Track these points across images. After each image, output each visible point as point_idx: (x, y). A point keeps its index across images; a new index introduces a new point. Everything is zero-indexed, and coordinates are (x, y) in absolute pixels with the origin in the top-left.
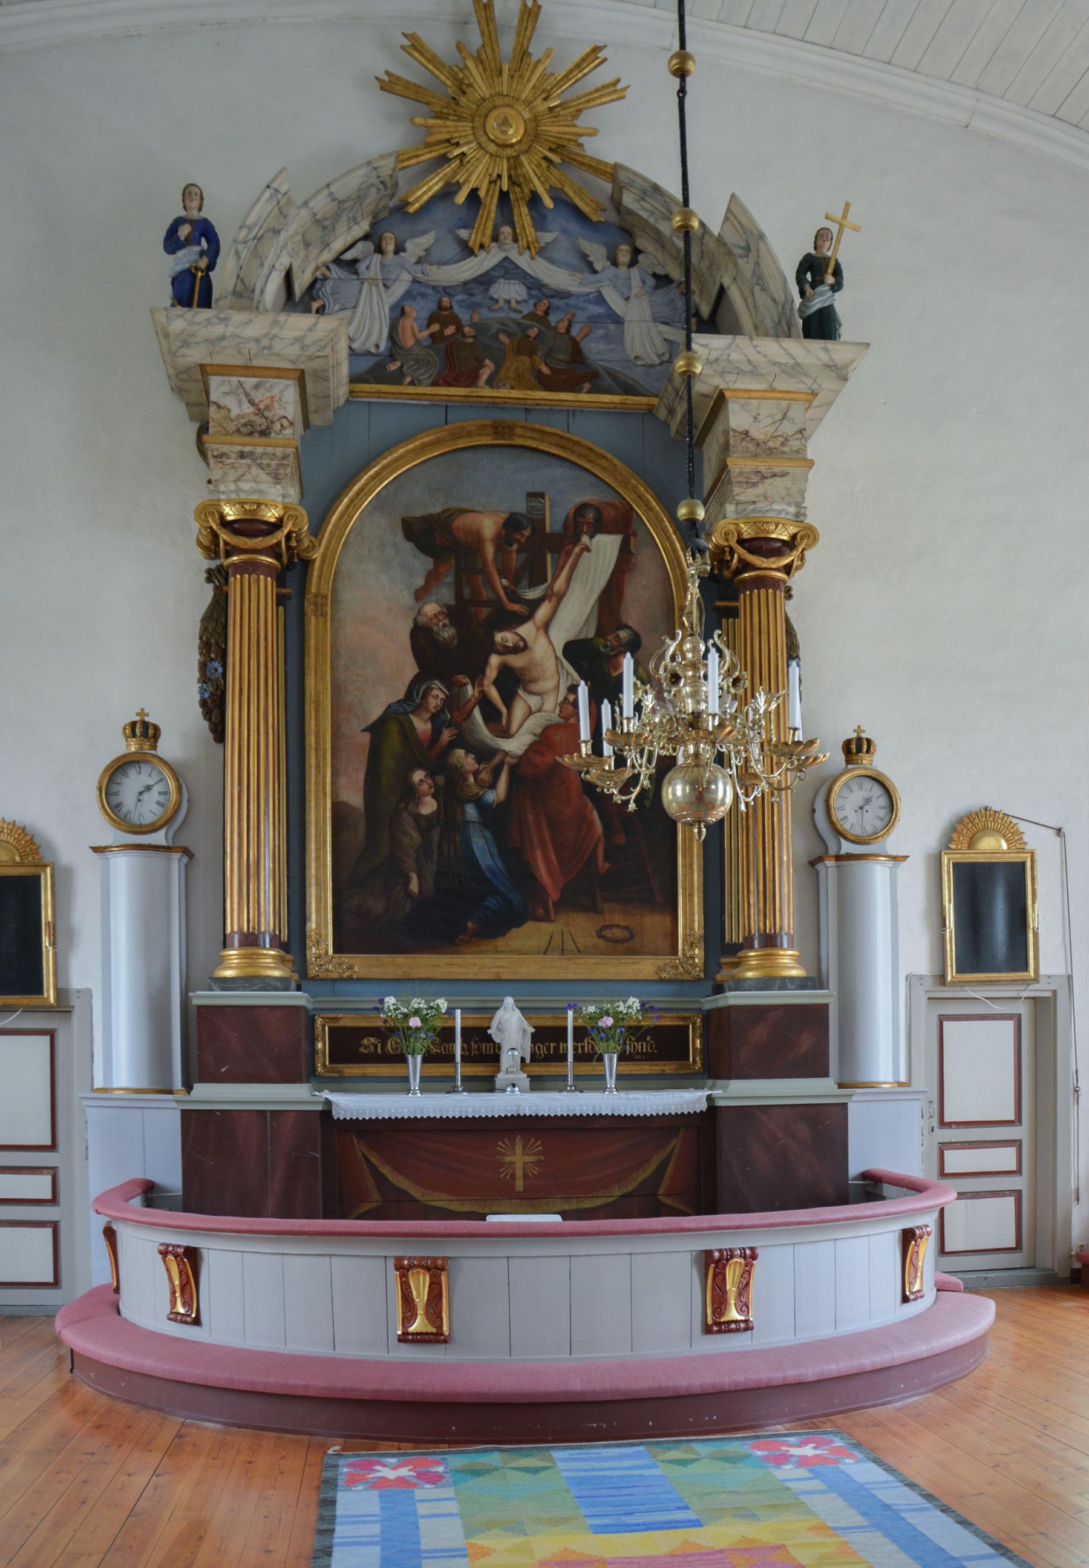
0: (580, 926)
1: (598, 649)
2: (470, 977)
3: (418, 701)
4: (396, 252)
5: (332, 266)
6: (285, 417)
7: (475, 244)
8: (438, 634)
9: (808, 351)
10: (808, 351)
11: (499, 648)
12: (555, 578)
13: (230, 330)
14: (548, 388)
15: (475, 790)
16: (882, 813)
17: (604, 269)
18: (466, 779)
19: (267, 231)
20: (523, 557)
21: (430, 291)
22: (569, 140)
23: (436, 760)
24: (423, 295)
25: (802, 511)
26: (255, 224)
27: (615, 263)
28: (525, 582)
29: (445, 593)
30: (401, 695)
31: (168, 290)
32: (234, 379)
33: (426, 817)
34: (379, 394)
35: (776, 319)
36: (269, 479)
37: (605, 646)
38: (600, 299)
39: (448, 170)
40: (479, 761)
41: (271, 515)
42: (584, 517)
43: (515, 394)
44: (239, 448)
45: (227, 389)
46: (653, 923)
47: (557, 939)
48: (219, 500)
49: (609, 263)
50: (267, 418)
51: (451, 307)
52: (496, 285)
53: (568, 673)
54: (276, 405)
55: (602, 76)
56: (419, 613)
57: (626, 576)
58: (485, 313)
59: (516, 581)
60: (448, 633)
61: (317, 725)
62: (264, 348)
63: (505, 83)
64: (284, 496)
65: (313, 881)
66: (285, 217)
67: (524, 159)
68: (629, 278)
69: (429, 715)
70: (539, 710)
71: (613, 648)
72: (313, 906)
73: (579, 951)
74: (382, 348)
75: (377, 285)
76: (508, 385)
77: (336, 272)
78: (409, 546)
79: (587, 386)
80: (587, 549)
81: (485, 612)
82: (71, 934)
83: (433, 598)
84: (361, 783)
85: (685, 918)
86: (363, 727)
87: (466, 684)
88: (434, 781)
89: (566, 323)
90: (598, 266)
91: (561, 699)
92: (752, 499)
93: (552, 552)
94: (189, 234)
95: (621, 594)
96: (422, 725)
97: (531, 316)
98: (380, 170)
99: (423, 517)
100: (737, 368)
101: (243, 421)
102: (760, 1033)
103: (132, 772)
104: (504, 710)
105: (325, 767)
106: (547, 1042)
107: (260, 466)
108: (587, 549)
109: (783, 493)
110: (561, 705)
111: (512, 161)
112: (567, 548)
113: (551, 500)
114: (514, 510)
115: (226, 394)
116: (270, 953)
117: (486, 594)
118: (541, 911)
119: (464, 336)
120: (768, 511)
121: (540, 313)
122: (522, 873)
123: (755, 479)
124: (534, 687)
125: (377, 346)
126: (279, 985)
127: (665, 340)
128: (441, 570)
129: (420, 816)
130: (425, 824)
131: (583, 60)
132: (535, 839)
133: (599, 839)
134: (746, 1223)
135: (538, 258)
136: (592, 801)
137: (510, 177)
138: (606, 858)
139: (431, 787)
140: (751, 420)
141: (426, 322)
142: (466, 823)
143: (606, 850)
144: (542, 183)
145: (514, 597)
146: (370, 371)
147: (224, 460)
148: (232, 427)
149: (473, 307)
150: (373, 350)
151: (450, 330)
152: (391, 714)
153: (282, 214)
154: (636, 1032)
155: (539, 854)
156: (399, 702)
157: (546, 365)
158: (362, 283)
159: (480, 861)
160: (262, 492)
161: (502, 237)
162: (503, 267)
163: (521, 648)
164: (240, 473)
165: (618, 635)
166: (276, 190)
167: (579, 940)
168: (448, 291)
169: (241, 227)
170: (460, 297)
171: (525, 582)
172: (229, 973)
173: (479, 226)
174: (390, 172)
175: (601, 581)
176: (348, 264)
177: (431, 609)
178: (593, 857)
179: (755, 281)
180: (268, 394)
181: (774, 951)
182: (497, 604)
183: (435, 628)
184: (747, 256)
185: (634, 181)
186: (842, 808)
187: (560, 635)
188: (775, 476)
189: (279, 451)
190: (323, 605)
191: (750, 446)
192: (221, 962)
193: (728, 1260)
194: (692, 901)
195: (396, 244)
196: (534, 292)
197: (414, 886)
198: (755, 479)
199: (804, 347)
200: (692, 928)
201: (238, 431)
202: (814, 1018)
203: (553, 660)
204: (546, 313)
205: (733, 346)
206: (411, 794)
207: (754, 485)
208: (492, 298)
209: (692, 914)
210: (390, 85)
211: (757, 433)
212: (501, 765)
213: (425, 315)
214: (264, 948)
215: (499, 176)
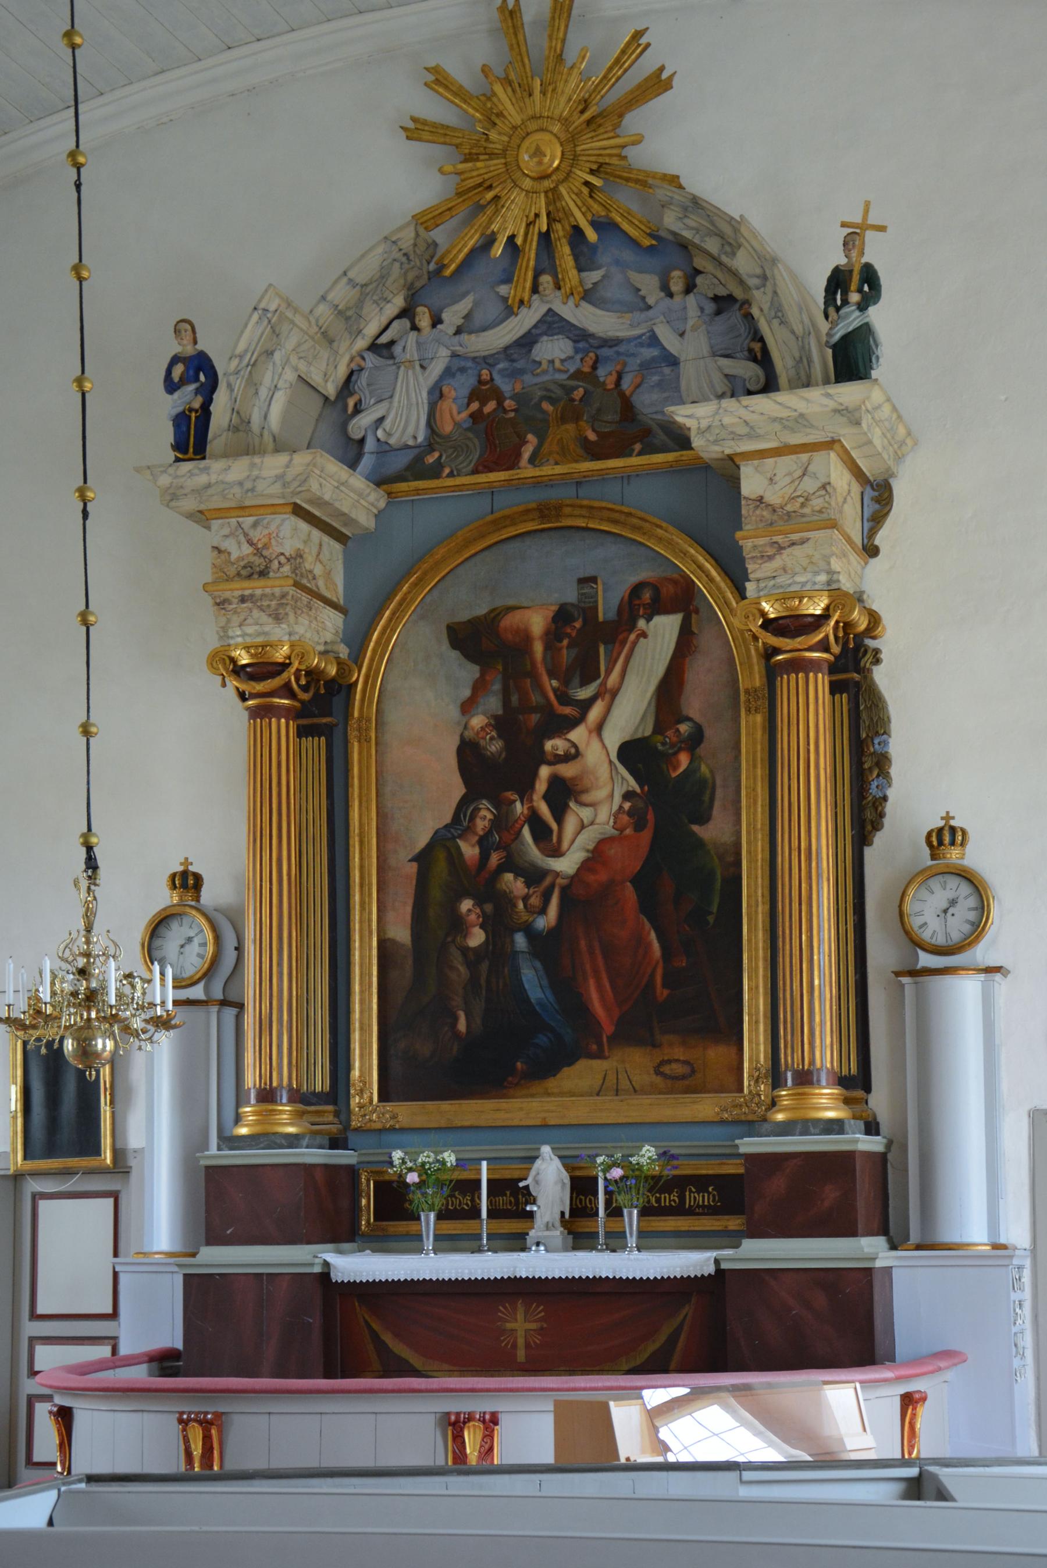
0: (636, 1063)
1: (656, 748)
2: (516, 1122)
3: (465, 824)
4: (434, 326)
5: (366, 355)
6: (282, 554)
7: (514, 300)
8: (485, 749)
9: (807, 400)
10: (807, 400)
11: (550, 758)
12: (609, 672)
13: (214, 478)
14: (596, 457)
15: (525, 917)
16: (972, 916)
17: (657, 303)
18: (515, 906)
19: (260, 355)
20: (574, 652)
21: (470, 364)
22: (610, 155)
23: (484, 887)
24: (462, 370)
25: (835, 577)
26: (246, 351)
27: (670, 295)
28: (576, 680)
29: (493, 703)
30: (448, 819)
31: (168, 434)
32: (233, 521)
33: (474, 949)
34: (417, 491)
35: (797, 355)
36: (270, 620)
37: (664, 744)
38: (654, 340)
39: (483, 219)
40: (528, 885)
41: (280, 654)
42: (639, 598)
43: (559, 469)
44: (240, 593)
45: (226, 531)
46: (716, 1054)
47: (611, 1078)
48: (229, 645)
49: (662, 294)
50: (265, 557)
51: (492, 379)
52: (539, 345)
53: (623, 778)
54: (273, 542)
55: (647, 65)
56: (466, 727)
57: (687, 660)
58: (529, 379)
59: (566, 682)
60: (495, 747)
61: (361, 859)
62: (248, 491)
63: (538, 102)
64: (290, 634)
65: (357, 1025)
66: (277, 336)
67: (563, 190)
68: (685, 308)
69: (477, 838)
70: (592, 823)
71: (672, 745)
72: (357, 1052)
73: (635, 1091)
74: (420, 439)
75: (414, 368)
76: (552, 461)
77: (370, 357)
78: (455, 654)
79: (638, 447)
80: (644, 635)
81: (535, 718)
82: (129, 1091)
83: (480, 710)
84: (408, 918)
85: (751, 1049)
86: (410, 857)
87: (514, 801)
88: (482, 910)
89: (614, 376)
90: (651, 301)
91: (615, 808)
92: (769, 574)
93: (605, 644)
94: (182, 374)
95: (681, 684)
96: (469, 850)
97: (578, 375)
98: (399, 243)
99: (469, 621)
100: (732, 433)
101: (242, 564)
102: (778, 1185)
103: (175, 925)
104: (554, 826)
105: (370, 903)
106: (582, 1187)
107: (261, 609)
108: (644, 635)
109: (805, 562)
110: (616, 816)
111: (550, 195)
112: (621, 637)
113: (604, 584)
114: (564, 600)
115: (226, 536)
116: (285, 1108)
117: (535, 698)
118: (595, 1047)
119: (505, 411)
120: (790, 585)
121: (587, 369)
122: (575, 1009)
123: (770, 552)
124: (586, 798)
125: (415, 438)
126: (283, 1142)
127: (726, 376)
128: (488, 678)
129: (468, 948)
130: (473, 958)
131: (623, 52)
132: (588, 967)
133: (657, 963)
134: (480, 1386)
135: (584, 304)
136: (649, 920)
137: (548, 214)
138: (665, 985)
139: (479, 917)
140: (766, 482)
141: (466, 400)
142: (515, 953)
143: (665, 976)
144: (584, 214)
145: (564, 698)
146: (409, 468)
147: (226, 606)
148: (232, 571)
149: (514, 374)
150: (411, 443)
151: (491, 406)
152: (443, 841)
153: (275, 333)
154: (657, 1184)
155: (592, 983)
156: (446, 826)
157: (594, 430)
158: (399, 368)
159: (529, 993)
160: (266, 634)
161: (541, 288)
162: (545, 322)
163: (573, 755)
164: (242, 618)
165: (678, 730)
166: (265, 310)
167: (634, 1079)
168: (488, 361)
169: (231, 358)
170: (501, 366)
171: (576, 680)
172: (243, 1131)
173: (518, 277)
174: (412, 242)
175: (659, 669)
176: (381, 348)
177: (478, 721)
178: (651, 984)
179: (773, 314)
180: (266, 532)
181: (806, 1090)
182: (546, 709)
183: (482, 743)
184: (764, 286)
185: (672, 198)
186: (919, 914)
187: (615, 736)
188: (793, 544)
189: (277, 591)
190: (368, 729)
191: (765, 513)
192: (238, 1119)
193: (464, 1423)
194: (757, 1029)
195: (431, 317)
196: (581, 345)
197: (462, 1026)
198: (770, 552)
199: (803, 398)
200: (758, 1061)
201: (238, 574)
202: (841, 1164)
203: (606, 765)
204: (594, 367)
205: (721, 411)
206: (458, 926)
207: (771, 558)
208: (534, 361)
209: (758, 1044)
210: (418, 130)
211: (773, 498)
212: (552, 886)
213: (465, 392)
214: (282, 1104)
215: (537, 215)
